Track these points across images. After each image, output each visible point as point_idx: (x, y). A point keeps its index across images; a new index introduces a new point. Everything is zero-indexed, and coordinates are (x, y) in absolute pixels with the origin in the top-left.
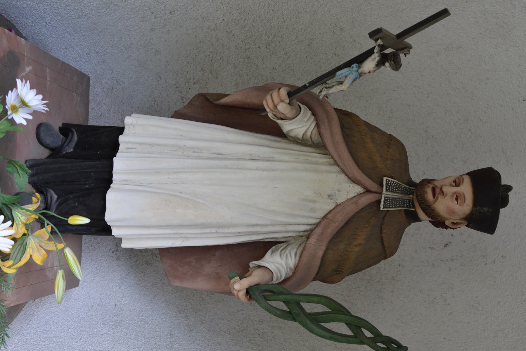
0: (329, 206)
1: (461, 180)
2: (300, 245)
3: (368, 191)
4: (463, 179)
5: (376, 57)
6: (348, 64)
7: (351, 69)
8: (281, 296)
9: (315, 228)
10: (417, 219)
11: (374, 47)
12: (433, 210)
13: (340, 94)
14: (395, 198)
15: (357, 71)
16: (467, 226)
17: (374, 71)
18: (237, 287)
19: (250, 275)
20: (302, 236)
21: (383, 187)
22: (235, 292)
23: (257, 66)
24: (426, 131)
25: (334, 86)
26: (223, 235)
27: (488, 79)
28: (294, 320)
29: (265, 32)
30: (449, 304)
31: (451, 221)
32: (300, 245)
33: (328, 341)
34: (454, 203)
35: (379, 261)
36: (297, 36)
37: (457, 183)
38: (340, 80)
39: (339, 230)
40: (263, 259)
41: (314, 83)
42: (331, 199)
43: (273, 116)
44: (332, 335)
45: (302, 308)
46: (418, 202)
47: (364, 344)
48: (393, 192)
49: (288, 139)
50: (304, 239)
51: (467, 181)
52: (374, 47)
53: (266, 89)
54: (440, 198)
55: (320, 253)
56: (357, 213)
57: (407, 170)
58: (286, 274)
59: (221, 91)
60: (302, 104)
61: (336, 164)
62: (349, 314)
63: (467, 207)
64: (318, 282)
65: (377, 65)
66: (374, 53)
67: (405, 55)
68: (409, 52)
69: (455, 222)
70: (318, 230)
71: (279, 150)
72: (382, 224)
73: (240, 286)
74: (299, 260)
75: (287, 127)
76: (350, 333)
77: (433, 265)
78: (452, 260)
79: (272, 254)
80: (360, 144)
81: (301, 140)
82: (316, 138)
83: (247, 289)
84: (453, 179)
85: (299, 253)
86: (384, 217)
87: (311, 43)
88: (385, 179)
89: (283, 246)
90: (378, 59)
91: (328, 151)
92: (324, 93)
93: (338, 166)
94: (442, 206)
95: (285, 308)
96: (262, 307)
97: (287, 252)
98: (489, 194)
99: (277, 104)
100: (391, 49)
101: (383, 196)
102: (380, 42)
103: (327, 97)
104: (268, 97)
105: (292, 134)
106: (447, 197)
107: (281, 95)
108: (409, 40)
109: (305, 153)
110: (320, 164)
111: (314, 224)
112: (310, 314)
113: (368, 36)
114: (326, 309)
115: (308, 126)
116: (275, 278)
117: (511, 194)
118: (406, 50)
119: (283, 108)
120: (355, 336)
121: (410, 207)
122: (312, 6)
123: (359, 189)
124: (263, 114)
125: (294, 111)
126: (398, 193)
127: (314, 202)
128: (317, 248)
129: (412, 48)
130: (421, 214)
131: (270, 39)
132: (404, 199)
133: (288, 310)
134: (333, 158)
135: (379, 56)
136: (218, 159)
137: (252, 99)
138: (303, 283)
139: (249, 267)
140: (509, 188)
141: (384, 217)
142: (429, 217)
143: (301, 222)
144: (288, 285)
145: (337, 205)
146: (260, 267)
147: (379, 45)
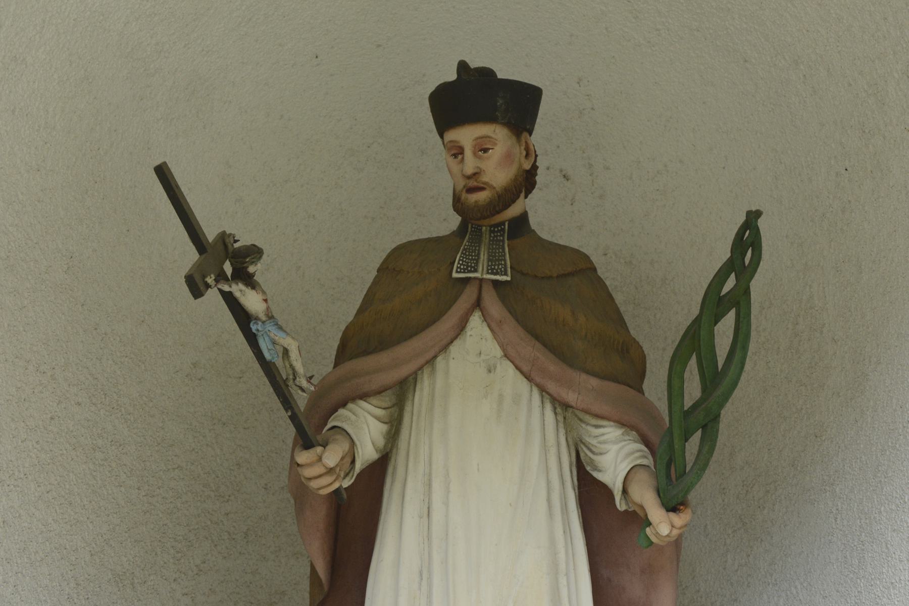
0: (508, 370)
1: (452, 144)
2: (581, 420)
3: (478, 304)
4: (451, 142)
5: (238, 289)
6: (252, 339)
7: (260, 334)
8: (676, 447)
9: (548, 393)
10: (523, 219)
11: (220, 291)
12: (506, 190)
13: (308, 358)
14: (489, 256)
15: (263, 322)
16: (530, 135)
17: (264, 293)
18: (664, 530)
19: (642, 507)
20: (565, 418)
21: (470, 278)
22: (675, 532)
23: (261, 518)
24: (373, 219)
25: (291, 365)
26: (571, 563)
27: (282, 116)
28: (716, 418)
29: (199, 504)
30: (666, 166)
31: (523, 159)
32: (581, 420)
33: (748, 366)
34: (491, 151)
35: (600, 280)
36: (207, 445)
37: (457, 152)
38: (281, 355)
39: (550, 351)
40: (610, 485)
41: (287, 402)
42: (495, 368)
43: (348, 478)
44: (739, 345)
45: (695, 406)
46: (493, 215)
47: (749, 288)
48: (477, 261)
49: (391, 450)
50: (569, 414)
51: (453, 135)
52: (220, 291)
53: (300, 491)
54: (485, 178)
55: (594, 382)
56: (517, 320)
57: (438, 240)
58: (635, 442)
59: (306, 585)
60: (326, 424)
61: (431, 361)
62: (697, 321)
63: (498, 134)
64: (646, 386)
65: (253, 288)
66: (230, 293)
67: (236, 241)
68: (230, 234)
69: (524, 153)
70: (552, 387)
71: (411, 465)
72: (536, 276)
73: (663, 525)
74: (609, 419)
75: (367, 453)
76: (731, 315)
77: (601, 197)
78: (591, 166)
79: (600, 471)
80: (397, 317)
81: (392, 426)
82: (387, 399)
83: (668, 510)
84: (451, 160)
85: (594, 421)
86: (523, 274)
87: (220, 420)
88: (455, 275)
89: (584, 451)
90: (241, 286)
91: (410, 375)
92: (304, 384)
93: (435, 357)
94: (498, 174)
95: (697, 436)
96: (699, 480)
97: (594, 442)
98: (477, 98)
99: (325, 469)
100: (224, 262)
101: (485, 276)
102: (210, 280)
103: (311, 378)
104: (314, 484)
105: (381, 442)
106: (483, 166)
107: (308, 461)
108: (211, 234)
109: (415, 418)
110: (433, 389)
111: (542, 397)
112: (704, 389)
113: (200, 300)
114: (693, 362)
115: (366, 414)
116: (645, 462)
117: (474, 63)
118: (227, 241)
119: (332, 456)
120: (737, 304)
121: (503, 230)
122: (153, 416)
123: (476, 320)
124: (345, 496)
125: (338, 437)
126: (479, 250)
127: (501, 397)
128: (583, 389)
129: (224, 233)
130: (514, 211)
131: (212, 494)
132: (490, 240)
133: (699, 433)
134: (421, 368)
135: (237, 284)
136: (430, 578)
137: (319, 516)
138: (649, 411)
139: (626, 511)
140: (463, 66)
141: (523, 274)
142: (518, 197)
143: (537, 421)
144: (654, 439)
145: (506, 356)
146: (625, 491)
147: (217, 281)
